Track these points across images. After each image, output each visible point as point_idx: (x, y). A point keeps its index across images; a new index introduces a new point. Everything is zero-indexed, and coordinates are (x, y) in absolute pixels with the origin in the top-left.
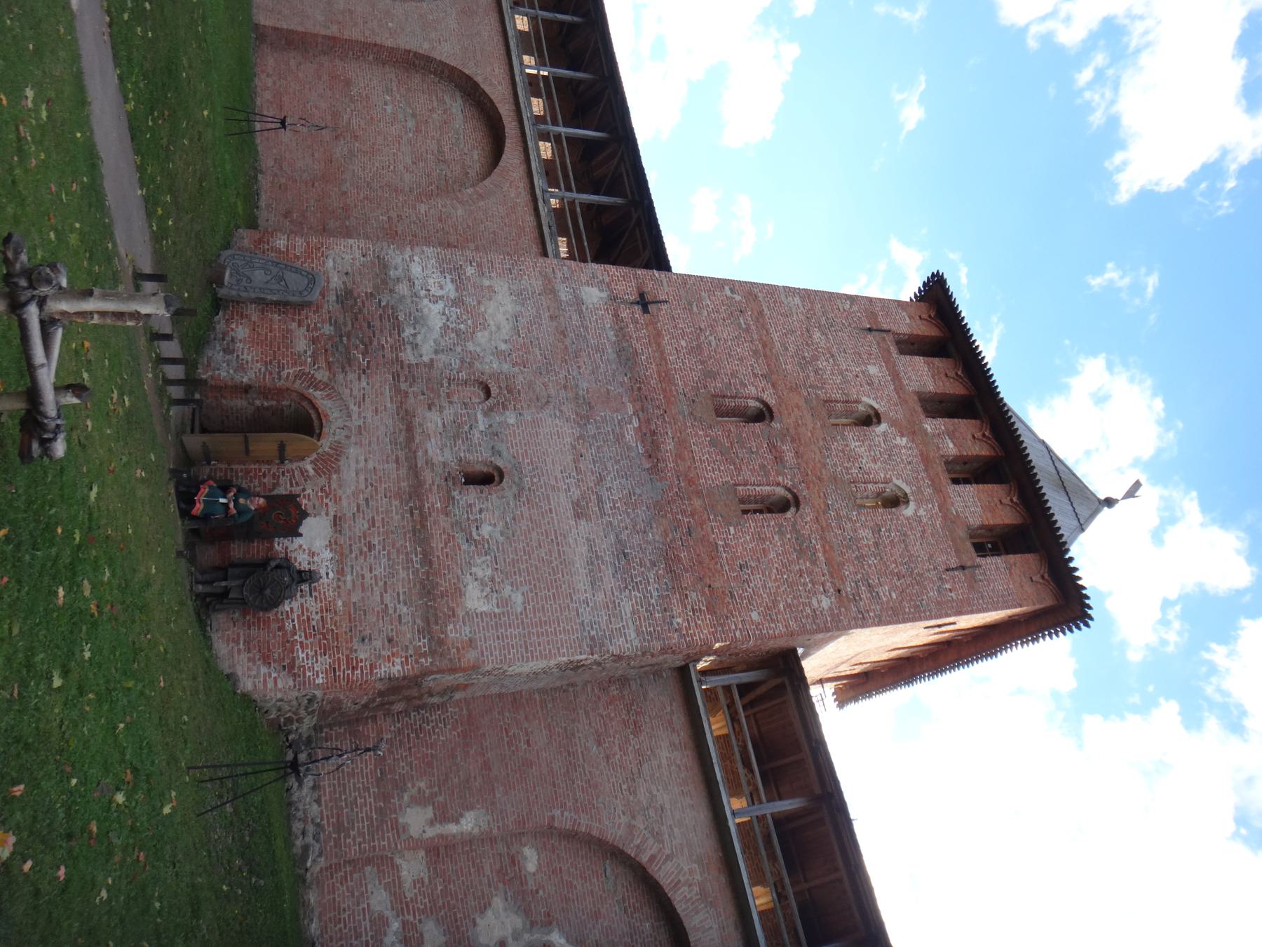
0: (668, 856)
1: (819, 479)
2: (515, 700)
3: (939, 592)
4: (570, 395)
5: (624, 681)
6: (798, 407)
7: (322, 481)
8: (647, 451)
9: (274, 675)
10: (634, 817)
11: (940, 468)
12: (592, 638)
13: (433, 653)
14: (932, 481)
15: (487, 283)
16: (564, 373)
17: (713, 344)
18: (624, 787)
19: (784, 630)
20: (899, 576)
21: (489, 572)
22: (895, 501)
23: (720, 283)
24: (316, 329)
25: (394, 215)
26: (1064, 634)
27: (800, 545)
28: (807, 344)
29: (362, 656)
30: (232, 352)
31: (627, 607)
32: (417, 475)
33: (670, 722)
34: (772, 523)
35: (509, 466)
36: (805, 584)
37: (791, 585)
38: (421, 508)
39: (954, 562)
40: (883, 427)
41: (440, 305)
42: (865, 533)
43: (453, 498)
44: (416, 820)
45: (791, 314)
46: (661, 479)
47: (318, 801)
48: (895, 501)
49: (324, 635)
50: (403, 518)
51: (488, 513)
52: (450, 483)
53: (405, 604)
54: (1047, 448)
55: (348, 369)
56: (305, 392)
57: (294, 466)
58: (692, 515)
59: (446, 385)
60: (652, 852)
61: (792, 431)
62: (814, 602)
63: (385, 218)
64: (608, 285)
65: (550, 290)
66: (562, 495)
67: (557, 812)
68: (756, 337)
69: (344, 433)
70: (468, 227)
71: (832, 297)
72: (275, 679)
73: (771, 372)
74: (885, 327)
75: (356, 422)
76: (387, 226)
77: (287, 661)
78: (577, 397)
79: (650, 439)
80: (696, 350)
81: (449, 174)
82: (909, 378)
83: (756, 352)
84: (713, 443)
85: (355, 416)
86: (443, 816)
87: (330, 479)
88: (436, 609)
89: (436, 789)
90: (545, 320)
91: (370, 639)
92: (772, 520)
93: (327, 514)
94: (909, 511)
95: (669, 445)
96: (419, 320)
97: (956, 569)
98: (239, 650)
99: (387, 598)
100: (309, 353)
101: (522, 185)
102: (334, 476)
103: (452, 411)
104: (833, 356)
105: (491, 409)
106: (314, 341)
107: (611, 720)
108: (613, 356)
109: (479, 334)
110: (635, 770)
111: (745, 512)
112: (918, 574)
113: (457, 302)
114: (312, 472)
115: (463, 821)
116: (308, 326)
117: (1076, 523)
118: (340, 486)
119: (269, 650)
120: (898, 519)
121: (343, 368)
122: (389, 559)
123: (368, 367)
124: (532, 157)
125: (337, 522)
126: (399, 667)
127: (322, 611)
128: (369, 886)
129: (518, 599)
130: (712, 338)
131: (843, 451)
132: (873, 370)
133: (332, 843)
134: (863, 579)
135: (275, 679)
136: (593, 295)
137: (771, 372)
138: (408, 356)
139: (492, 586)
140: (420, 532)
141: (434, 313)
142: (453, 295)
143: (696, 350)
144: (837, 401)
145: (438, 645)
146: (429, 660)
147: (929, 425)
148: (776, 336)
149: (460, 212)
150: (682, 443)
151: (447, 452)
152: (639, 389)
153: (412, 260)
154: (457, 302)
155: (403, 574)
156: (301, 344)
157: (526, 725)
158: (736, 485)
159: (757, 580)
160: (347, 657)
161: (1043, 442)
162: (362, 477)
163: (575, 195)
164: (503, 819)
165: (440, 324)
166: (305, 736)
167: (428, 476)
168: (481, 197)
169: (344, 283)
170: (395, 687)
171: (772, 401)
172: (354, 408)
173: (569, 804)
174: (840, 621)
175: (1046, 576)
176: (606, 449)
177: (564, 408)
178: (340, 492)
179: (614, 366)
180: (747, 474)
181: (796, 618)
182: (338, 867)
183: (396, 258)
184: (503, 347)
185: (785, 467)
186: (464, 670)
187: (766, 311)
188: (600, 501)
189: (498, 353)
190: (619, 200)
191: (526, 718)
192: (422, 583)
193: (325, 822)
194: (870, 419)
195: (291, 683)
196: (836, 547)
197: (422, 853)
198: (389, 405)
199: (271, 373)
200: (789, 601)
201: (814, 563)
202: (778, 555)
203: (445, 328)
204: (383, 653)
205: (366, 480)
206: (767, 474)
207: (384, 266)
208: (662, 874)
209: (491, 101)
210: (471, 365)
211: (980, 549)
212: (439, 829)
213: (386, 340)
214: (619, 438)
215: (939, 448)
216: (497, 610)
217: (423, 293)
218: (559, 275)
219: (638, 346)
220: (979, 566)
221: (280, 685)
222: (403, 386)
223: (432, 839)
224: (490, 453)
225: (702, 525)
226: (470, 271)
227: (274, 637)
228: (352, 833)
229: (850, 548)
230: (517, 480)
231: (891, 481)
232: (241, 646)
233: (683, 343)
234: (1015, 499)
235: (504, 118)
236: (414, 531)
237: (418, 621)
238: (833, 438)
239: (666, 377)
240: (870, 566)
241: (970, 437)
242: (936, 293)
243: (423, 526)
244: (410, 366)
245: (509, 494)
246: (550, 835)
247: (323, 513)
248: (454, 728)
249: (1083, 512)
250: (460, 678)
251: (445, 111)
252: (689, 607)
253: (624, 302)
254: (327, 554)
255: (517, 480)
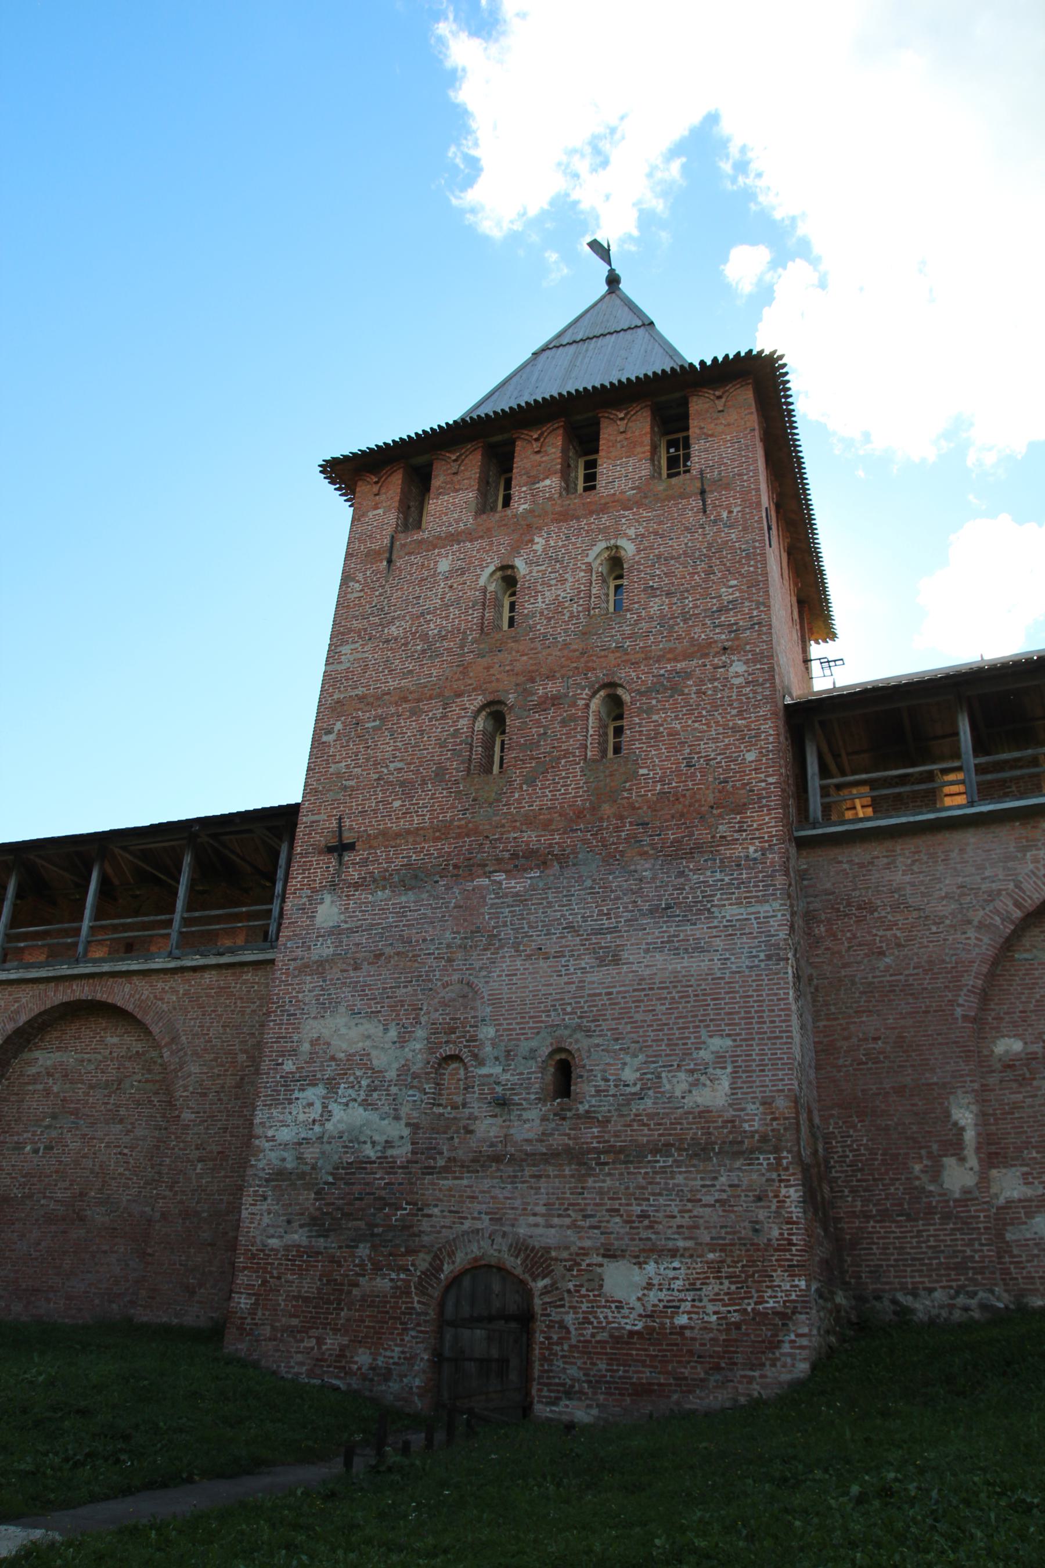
0: (1016, 886)
1: (583, 654)
2: (824, 1051)
3: (730, 527)
4: (460, 955)
5: (810, 917)
6: (488, 668)
7: (559, 1269)
8: (538, 867)
9: (793, 1337)
10: (969, 922)
11: (575, 501)
12: (769, 957)
13: (777, 1150)
14: (591, 513)
15: (306, 1047)
16: (430, 960)
17: (400, 765)
18: (934, 929)
19: (770, 724)
20: (709, 572)
21: (682, 1075)
22: (616, 563)
23: (317, 744)
24: (362, 1265)
25: (196, 1154)
26: (788, 382)
27: (666, 689)
28: (406, 644)
29: (776, 1233)
30: (389, 1370)
31: (732, 911)
32: (556, 1155)
33: (861, 865)
34: (637, 720)
35: (550, 1040)
36: (715, 690)
37: (716, 708)
38: (600, 1153)
39: (696, 503)
40: (519, 563)
41: (333, 1106)
42: (655, 606)
43: (587, 1112)
44: (958, 1177)
45: (364, 660)
46: (575, 852)
47: (931, 1291)
48: (616, 563)
49: (747, 1277)
50: (609, 1174)
51: (613, 1070)
52: (569, 1114)
53: (715, 1178)
54: (545, 349)
55: (416, 1229)
56: (443, 1284)
57: (537, 1301)
58: (621, 818)
59: (441, 1110)
60: (1010, 903)
61: (521, 679)
62: (737, 681)
63: (200, 1166)
64: (314, 891)
65: (320, 967)
66: (589, 978)
67: (959, 1011)
68: (393, 710)
69: (499, 1239)
70: (215, 1059)
71: (343, 604)
72: (797, 1335)
73: (440, 695)
74: (387, 541)
75: (485, 1223)
76: (210, 1164)
77: (778, 1321)
78: (463, 947)
79: (523, 861)
80: (406, 788)
81: (139, 1077)
82: (457, 521)
83: (414, 712)
84: (531, 781)
85: (479, 1225)
86: (954, 1146)
87: (556, 1259)
88: (724, 1143)
89: (923, 1152)
90: (360, 976)
91: (757, 1222)
92: (632, 720)
93: (601, 1265)
94: (629, 549)
95: (531, 837)
96: (353, 1139)
97: (704, 501)
98: (762, 1376)
99: (708, 1199)
100: (393, 1276)
101: (160, 985)
102: (553, 1254)
103: (476, 1105)
104: (422, 614)
105: (475, 1056)
106: (377, 1268)
107: (854, 937)
108: (411, 896)
109: (375, 1062)
110: (915, 914)
111: (617, 750)
112: (709, 548)
113: (331, 1086)
114: (547, 1281)
115: (962, 1123)
116: (357, 1275)
117: (641, 331)
118: (567, 1248)
119: (763, 1342)
120: (638, 563)
121: (415, 1235)
122: (660, 1194)
123: (415, 1204)
124: (124, 968)
125: (611, 1254)
126: (792, 1190)
127: (719, 1278)
128: (1028, 1236)
129: (717, 1043)
130: (392, 766)
131: (549, 619)
132: (444, 566)
133: (979, 1277)
134: (711, 616)
135: (797, 1335)
136: (328, 912)
137: (440, 695)
138: (402, 1152)
139: (699, 1074)
140: (628, 1155)
141: (346, 1116)
142: (321, 1090)
143: (406, 788)
144: (483, 617)
145: (768, 1142)
146: (785, 1154)
147: (521, 506)
148: (392, 684)
149: (194, 1069)
150: (530, 821)
151: (526, 1115)
152: (456, 866)
153: (273, 1139)
154: (331, 1086)
155: (680, 1179)
156: (383, 1284)
157: (855, 1040)
158: (585, 759)
159: (708, 748)
160: (776, 1250)
161: (536, 354)
162: (556, 1221)
163: (177, 917)
164: (962, 1076)
165: (361, 1110)
166: (853, 1303)
167: (558, 1141)
168: (174, 1039)
169: (301, 1226)
170: (811, 1198)
171: (480, 700)
172: (467, 1225)
173: (950, 996)
174: (762, 652)
175: (717, 393)
176: (532, 918)
177: (477, 965)
178: (574, 1249)
179: (425, 896)
180: (572, 745)
181: (755, 706)
182: (1005, 1272)
183: (268, 1157)
184: (393, 1033)
185: (566, 695)
186: (797, 1113)
187: (360, 691)
188: (599, 932)
189: (402, 1041)
190: (187, 860)
191: (846, 1039)
192: (691, 1157)
193: (954, 1284)
194: (509, 579)
195: (803, 1317)
196: (671, 645)
197: (994, 1172)
198: (465, 1182)
199: (418, 1324)
200: (734, 712)
201: (688, 675)
202: (677, 718)
203: (366, 1104)
204: (774, 1208)
205: (559, 1216)
206: (573, 718)
207: (280, 1175)
208: (1036, 896)
209: (40, 1014)
210: (415, 1076)
211: (676, 465)
212: (970, 1152)
213: (380, 1179)
214: (520, 899)
215: (550, 499)
216: (729, 1070)
217: (317, 1128)
218: (299, 953)
219: (399, 862)
220: (701, 472)
221: (806, 1330)
222: (441, 1163)
223: (980, 1160)
224: (532, 1063)
225: (634, 808)
226: (289, 1066)
227: (748, 1335)
228: (969, 1253)
229: (672, 627)
230: (567, 1032)
231: (589, 564)
232: (756, 1374)
233: (397, 804)
234: (622, 415)
235: (66, 999)
236: (625, 1162)
237: (738, 1164)
238: (531, 628)
239: (442, 831)
240: (696, 607)
241: (538, 457)
242: (347, 472)
243: (621, 1150)
244: (413, 1153)
245: (585, 1043)
246: (983, 1024)
247: (599, 1270)
248: (854, 1126)
249: (626, 320)
250: (803, 1116)
251: (49, 1074)
252: (736, 835)
253: (338, 873)
254: (651, 1268)
255: (567, 1032)
